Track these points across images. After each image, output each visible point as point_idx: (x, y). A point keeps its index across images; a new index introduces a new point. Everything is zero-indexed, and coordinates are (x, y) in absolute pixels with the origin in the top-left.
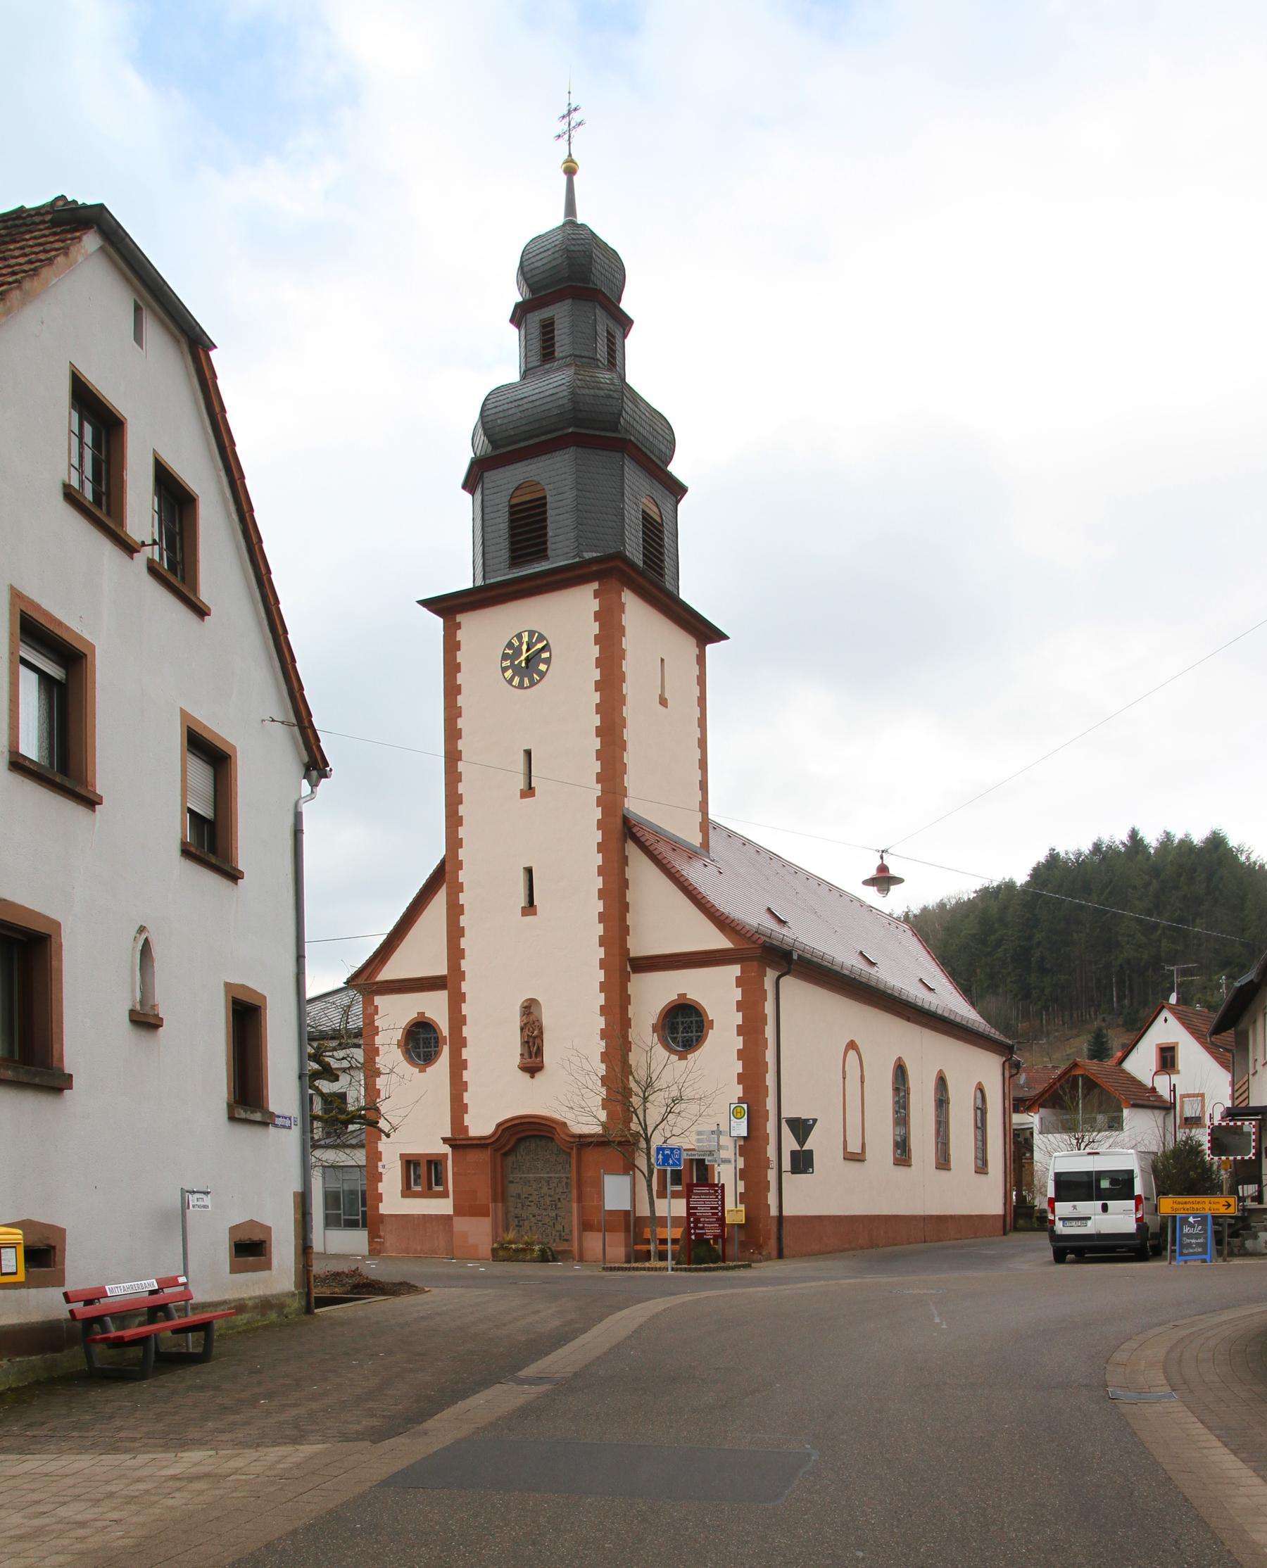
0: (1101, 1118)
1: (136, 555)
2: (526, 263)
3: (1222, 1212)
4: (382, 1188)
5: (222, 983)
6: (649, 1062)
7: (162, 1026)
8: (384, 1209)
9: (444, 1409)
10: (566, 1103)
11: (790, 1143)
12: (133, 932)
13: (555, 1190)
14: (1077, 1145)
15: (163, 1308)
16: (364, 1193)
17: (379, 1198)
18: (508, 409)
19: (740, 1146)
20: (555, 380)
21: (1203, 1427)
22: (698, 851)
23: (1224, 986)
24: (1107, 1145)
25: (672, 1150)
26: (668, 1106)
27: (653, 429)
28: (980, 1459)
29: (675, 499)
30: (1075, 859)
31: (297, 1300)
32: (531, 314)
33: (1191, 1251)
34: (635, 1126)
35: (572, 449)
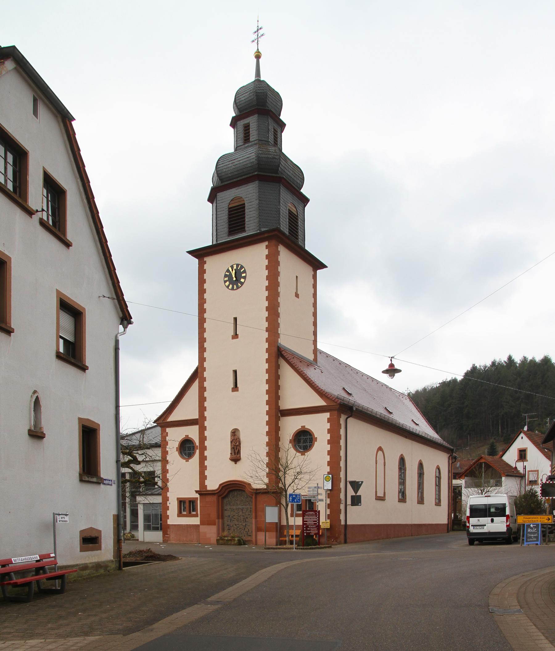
0: (492, 481)
1: (33, 216)
2: (237, 99)
3: (545, 522)
4: (169, 513)
5: (77, 418)
6: (287, 456)
7: (45, 437)
8: (169, 522)
9: (165, 618)
10: (250, 475)
11: (351, 492)
12: (31, 394)
13: (245, 514)
14: (481, 493)
15: (43, 568)
16: (161, 515)
17: (168, 517)
18: (228, 164)
19: (328, 493)
20: (250, 150)
21: (535, 628)
22: (312, 362)
23: (548, 422)
24: (495, 492)
25: (296, 495)
26: (295, 476)
27: (294, 173)
28: (422, 646)
29: (304, 205)
30: (483, 369)
31: (114, 564)
32: (239, 122)
33: (531, 540)
34: (280, 485)
35: (257, 182)
